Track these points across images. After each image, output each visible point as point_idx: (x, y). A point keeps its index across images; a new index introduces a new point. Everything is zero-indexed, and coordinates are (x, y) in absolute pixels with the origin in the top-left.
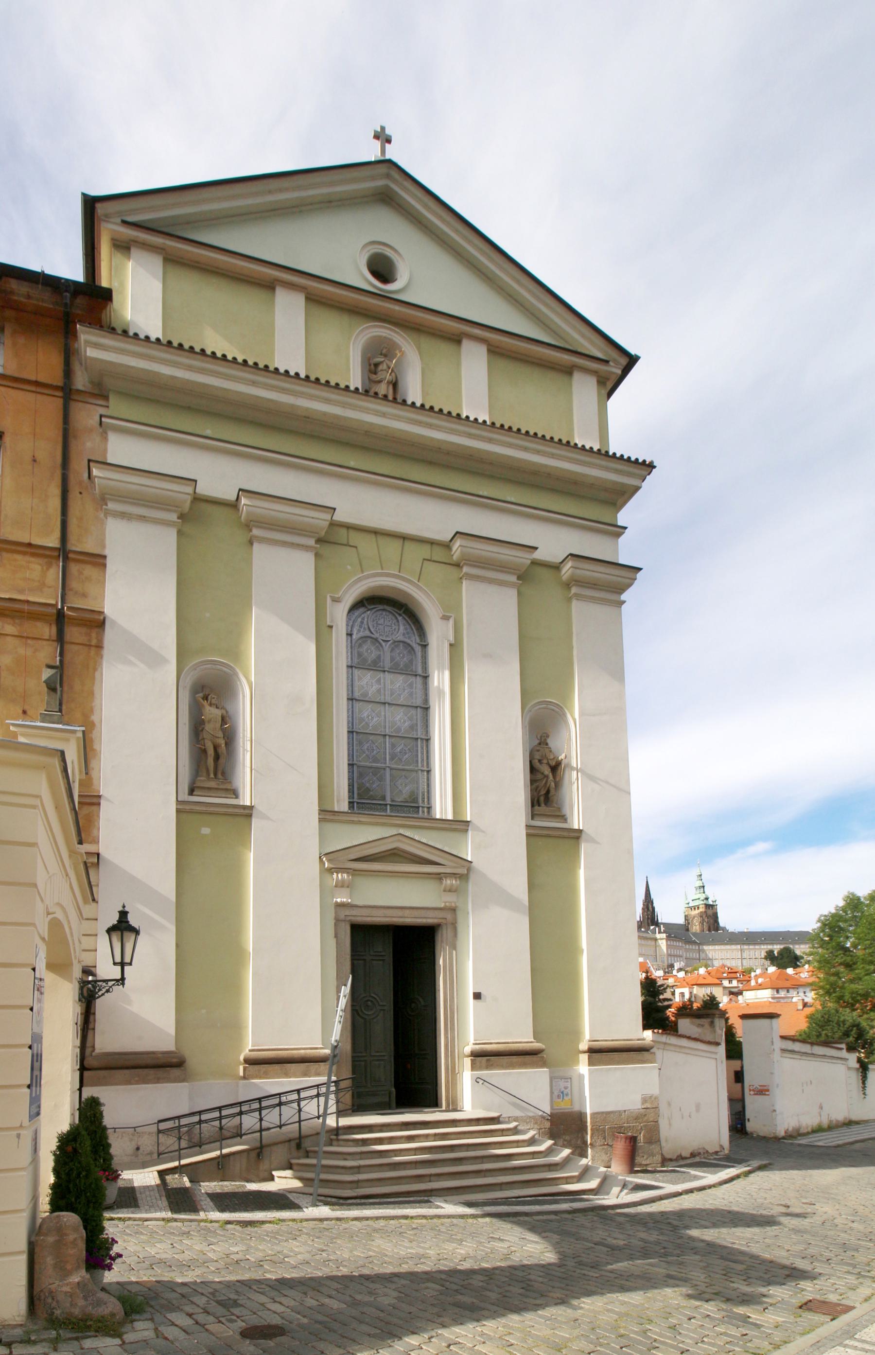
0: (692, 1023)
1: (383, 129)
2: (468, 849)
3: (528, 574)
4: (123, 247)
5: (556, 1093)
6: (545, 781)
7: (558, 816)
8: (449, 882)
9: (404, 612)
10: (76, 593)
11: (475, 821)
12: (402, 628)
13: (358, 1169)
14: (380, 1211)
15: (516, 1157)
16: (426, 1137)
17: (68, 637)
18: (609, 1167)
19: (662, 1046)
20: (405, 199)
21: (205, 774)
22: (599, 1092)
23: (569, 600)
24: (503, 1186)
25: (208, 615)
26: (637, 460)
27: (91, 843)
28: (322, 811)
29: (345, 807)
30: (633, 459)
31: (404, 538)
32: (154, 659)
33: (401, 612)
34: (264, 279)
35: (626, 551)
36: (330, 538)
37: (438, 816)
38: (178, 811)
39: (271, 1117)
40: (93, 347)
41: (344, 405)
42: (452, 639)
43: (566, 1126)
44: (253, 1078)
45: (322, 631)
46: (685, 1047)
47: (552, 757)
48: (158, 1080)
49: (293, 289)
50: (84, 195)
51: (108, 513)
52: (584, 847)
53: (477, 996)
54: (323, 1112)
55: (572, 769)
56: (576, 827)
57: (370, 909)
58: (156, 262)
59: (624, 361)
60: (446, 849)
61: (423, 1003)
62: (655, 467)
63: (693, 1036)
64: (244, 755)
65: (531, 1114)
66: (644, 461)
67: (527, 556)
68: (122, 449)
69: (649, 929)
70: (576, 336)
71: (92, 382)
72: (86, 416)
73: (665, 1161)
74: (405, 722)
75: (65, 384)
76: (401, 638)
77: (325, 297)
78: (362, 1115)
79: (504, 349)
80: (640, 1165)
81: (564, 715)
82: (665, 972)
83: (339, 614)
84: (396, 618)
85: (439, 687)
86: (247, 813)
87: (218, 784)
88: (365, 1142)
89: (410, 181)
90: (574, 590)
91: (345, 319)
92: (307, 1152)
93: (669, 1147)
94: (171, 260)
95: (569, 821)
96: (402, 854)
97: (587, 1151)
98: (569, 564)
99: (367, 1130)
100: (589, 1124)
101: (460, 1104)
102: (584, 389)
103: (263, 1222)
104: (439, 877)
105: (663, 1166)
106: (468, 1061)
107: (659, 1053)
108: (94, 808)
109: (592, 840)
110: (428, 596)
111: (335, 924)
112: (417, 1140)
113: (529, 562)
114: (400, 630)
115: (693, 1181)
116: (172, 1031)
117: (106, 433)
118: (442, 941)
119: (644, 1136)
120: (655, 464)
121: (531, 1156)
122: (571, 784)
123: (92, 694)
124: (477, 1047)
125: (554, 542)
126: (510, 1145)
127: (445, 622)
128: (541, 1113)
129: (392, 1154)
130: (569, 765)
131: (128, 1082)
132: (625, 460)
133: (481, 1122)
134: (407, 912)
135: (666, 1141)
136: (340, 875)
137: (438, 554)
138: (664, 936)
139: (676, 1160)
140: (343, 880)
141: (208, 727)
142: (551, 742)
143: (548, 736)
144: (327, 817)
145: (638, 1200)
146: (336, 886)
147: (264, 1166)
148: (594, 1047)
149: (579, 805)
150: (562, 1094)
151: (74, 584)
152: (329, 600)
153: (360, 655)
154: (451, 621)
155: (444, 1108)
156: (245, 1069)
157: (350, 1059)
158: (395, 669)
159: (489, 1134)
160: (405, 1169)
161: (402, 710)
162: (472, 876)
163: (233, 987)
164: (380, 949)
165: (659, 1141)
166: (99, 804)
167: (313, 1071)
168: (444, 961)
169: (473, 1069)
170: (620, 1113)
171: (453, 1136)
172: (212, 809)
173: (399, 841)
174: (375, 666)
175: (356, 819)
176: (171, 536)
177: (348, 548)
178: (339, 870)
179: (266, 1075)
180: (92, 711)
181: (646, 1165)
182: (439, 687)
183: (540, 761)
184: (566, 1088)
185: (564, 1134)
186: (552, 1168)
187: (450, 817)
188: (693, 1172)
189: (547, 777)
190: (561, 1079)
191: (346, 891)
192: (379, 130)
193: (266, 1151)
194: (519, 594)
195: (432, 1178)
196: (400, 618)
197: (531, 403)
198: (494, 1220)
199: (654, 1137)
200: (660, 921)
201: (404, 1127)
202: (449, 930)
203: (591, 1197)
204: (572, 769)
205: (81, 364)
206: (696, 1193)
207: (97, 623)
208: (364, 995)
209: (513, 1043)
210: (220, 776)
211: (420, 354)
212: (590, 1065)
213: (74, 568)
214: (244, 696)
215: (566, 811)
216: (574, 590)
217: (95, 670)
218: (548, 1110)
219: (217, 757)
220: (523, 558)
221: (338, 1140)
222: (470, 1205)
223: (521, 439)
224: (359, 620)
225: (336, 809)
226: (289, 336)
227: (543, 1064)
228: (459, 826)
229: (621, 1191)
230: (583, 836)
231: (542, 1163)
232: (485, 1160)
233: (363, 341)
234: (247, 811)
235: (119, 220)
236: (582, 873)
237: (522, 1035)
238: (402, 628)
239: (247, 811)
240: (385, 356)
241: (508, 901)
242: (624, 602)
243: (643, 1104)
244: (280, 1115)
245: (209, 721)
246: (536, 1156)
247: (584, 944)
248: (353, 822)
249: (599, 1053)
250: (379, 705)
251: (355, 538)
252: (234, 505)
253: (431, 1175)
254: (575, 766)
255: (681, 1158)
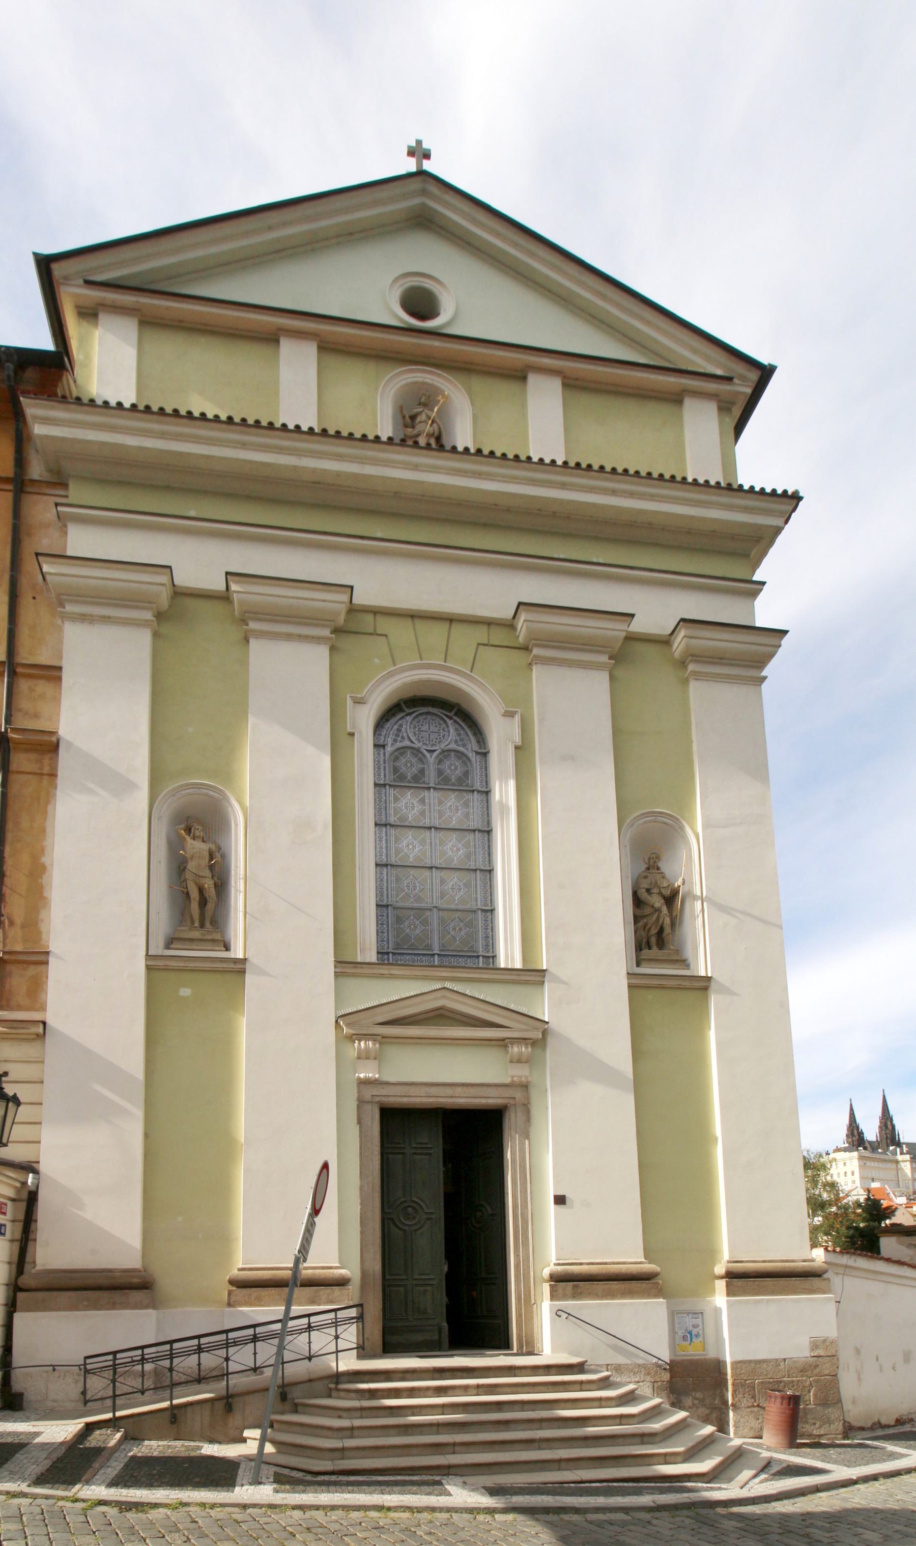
0: (901, 1243)
1: (419, 143)
2: (545, 1006)
3: (623, 651)
4: (89, 314)
5: (680, 1333)
6: (655, 918)
7: (677, 961)
8: (516, 1049)
9: (456, 714)
10: (26, 713)
11: (553, 970)
12: (452, 731)
13: (351, 1431)
14: (357, 1496)
15: (594, 1422)
16: (465, 1389)
17: (14, 766)
18: (761, 1438)
19: (841, 1271)
20: (452, 221)
21: (189, 924)
22: (738, 1332)
23: (685, 682)
24: (563, 1464)
25: (191, 729)
26: (774, 491)
27: (38, 1010)
28: (338, 962)
29: (372, 957)
30: (768, 490)
31: (451, 620)
32: (121, 785)
33: (451, 714)
34: (262, 330)
35: (766, 612)
36: (350, 626)
37: (502, 966)
38: (149, 968)
39: (242, 1357)
40: (46, 423)
41: (362, 461)
42: (518, 740)
43: (694, 1381)
44: (240, 1305)
45: (340, 741)
46: (882, 1273)
47: (665, 885)
48: (113, 1306)
49: (301, 338)
50: (35, 254)
51: (66, 617)
52: (714, 1000)
53: (560, 1200)
54: (339, 1349)
55: (695, 898)
56: (703, 974)
57: (408, 1088)
58: (130, 327)
59: (754, 376)
60: (512, 1007)
61: (490, 1211)
62: (800, 499)
63: (894, 1258)
64: (236, 898)
65: (641, 1362)
66: (785, 492)
67: (623, 627)
68: (82, 541)
69: (888, 1149)
70: (687, 354)
71: (50, 471)
72: (41, 509)
73: (849, 1430)
74: (458, 850)
75: (16, 473)
76: (453, 746)
77: (342, 342)
78: (392, 1358)
79: (583, 380)
80: (810, 1436)
81: (682, 828)
82: (909, 1199)
83: (364, 720)
84: (445, 722)
85: (501, 802)
86: (239, 968)
87: (203, 935)
88: (373, 1394)
89: (452, 193)
90: (691, 667)
91: (371, 367)
92: (296, 1405)
93: (854, 1413)
94: (149, 323)
95: (692, 966)
96: (451, 1015)
97: (728, 1415)
98: (682, 633)
99: (383, 1377)
100: (729, 1377)
101: (538, 1345)
102: (701, 422)
103: (156, 1506)
104: (503, 1043)
105: (846, 1437)
106: (546, 1288)
107: (836, 1281)
108: (42, 967)
109: (725, 990)
110: (480, 685)
111: (358, 1107)
112: (450, 1392)
113: (624, 634)
114: (452, 735)
115: (884, 1461)
116: (136, 1242)
117: (66, 526)
118: (510, 1128)
119: (815, 1395)
120: (801, 494)
121: (618, 1421)
122: (694, 918)
123: (43, 831)
124: (560, 1268)
125: (655, 610)
126: (588, 1404)
127: (508, 719)
128: (655, 1360)
129: (409, 1412)
130: (690, 894)
131: (74, 1307)
132: (757, 493)
133: (553, 1370)
134: (459, 1090)
135: (854, 1402)
136: (362, 1044)
137: (499, 636)
138: (908, 1157)
139: (872, 1428)
140: (367, 1049)
141: (191, 866)
142: (664, 866)
143: (658, 858)
144: (347, 970)
145: (774, 1492)
146: (359, 1058)
147: (235, 1420)
148: (735, 1270)
149: (705, 944)
150: (689, 1336)
151: (23, 703)
152: (349, 702)
153: (396, 770)
154: (517, 718)
155: (515, 1351)
156: (230, 1293)
157: (379, 1282)
158: (445, 783)
159: (561, 1388)
160: (421, 1434)
161: (454, 835)
162: (550, 1041)
163: (219, 1190)
164: (425, 1140)
165: (839, 1401)
166: (47, 963)
167: (324, 1297)
168: (513, 1154)
169: (553, 1297)
170: (777, 1362)
171: (505, 1389)
172: (191, 965)
173: (445, 997)
174: (418, 782)
175: (385, 972)
176: (144, 638)
177: (375, 637)
178: (361, 1037)
179: (259, 1302)
180: (42, 851)
181: (820, 1436)
182: (501, 802)
183: (648, 891)
184: (695, 1326)
185: (694, 1390)
186: (646, 1439)
187: (518, 965)
188: (890, 1447)
189: (658, 910)
190: (688, 1314)
191: (373, 1064)
192: (414, 144)
193: (237, 1403)
194: (612, 678)
195: (457, 1448)
196: (449, 722)
197: (625, 438)
198: (520, 1518)
199: (830, 1396)
200: (902, 1141)
201: (437, 1375)
202: (519, 1114)
203: (700, 1485)
204: (695, 898)
205: (37, 451)
206: (882, 1481)
207: (48, 746)
208: (403, 1199)
209: (614, 1263)
210: (208, 925)
211: (469, 395)
212: (728, 1295)
213: (23, 685)
214: (236, 825)
215: (688, 954)
216: (691, 667)
217: (47, 802)
218: (666, 1356)
219: (203, 902)
220: (615, 630)
221: (338, 1390)
222: (493, 1491)
223: (571, 475)
224: (396, 727)
225: (359, 960)
226: (295, 388)
227: (659, 1292)
228: (532, 976)
229: (755, 1476)
230: (713, 985)
231: (629, 1432)
232: (544, 1424)
233: (392, 392)
234: (239, 966)
235: (81, 282)
236: (712, 1035)
237: (629, 1254)
238: (452, 731)
239: (239, 966)
240: (425, 405)
241: (603, 1073)
242: (765, 678)
243: (812, 1350)
244: (255, 1354)
245: (192, 858)
246: (624, 1421)
247: (718, 1130)
248: (382, 976)
249: (742, 1279)
250: (422, 831)
251: (384, 625)
252: (225, 597)
253: (454, 1444)
254: (699, 894)
255: (879, 1425)
